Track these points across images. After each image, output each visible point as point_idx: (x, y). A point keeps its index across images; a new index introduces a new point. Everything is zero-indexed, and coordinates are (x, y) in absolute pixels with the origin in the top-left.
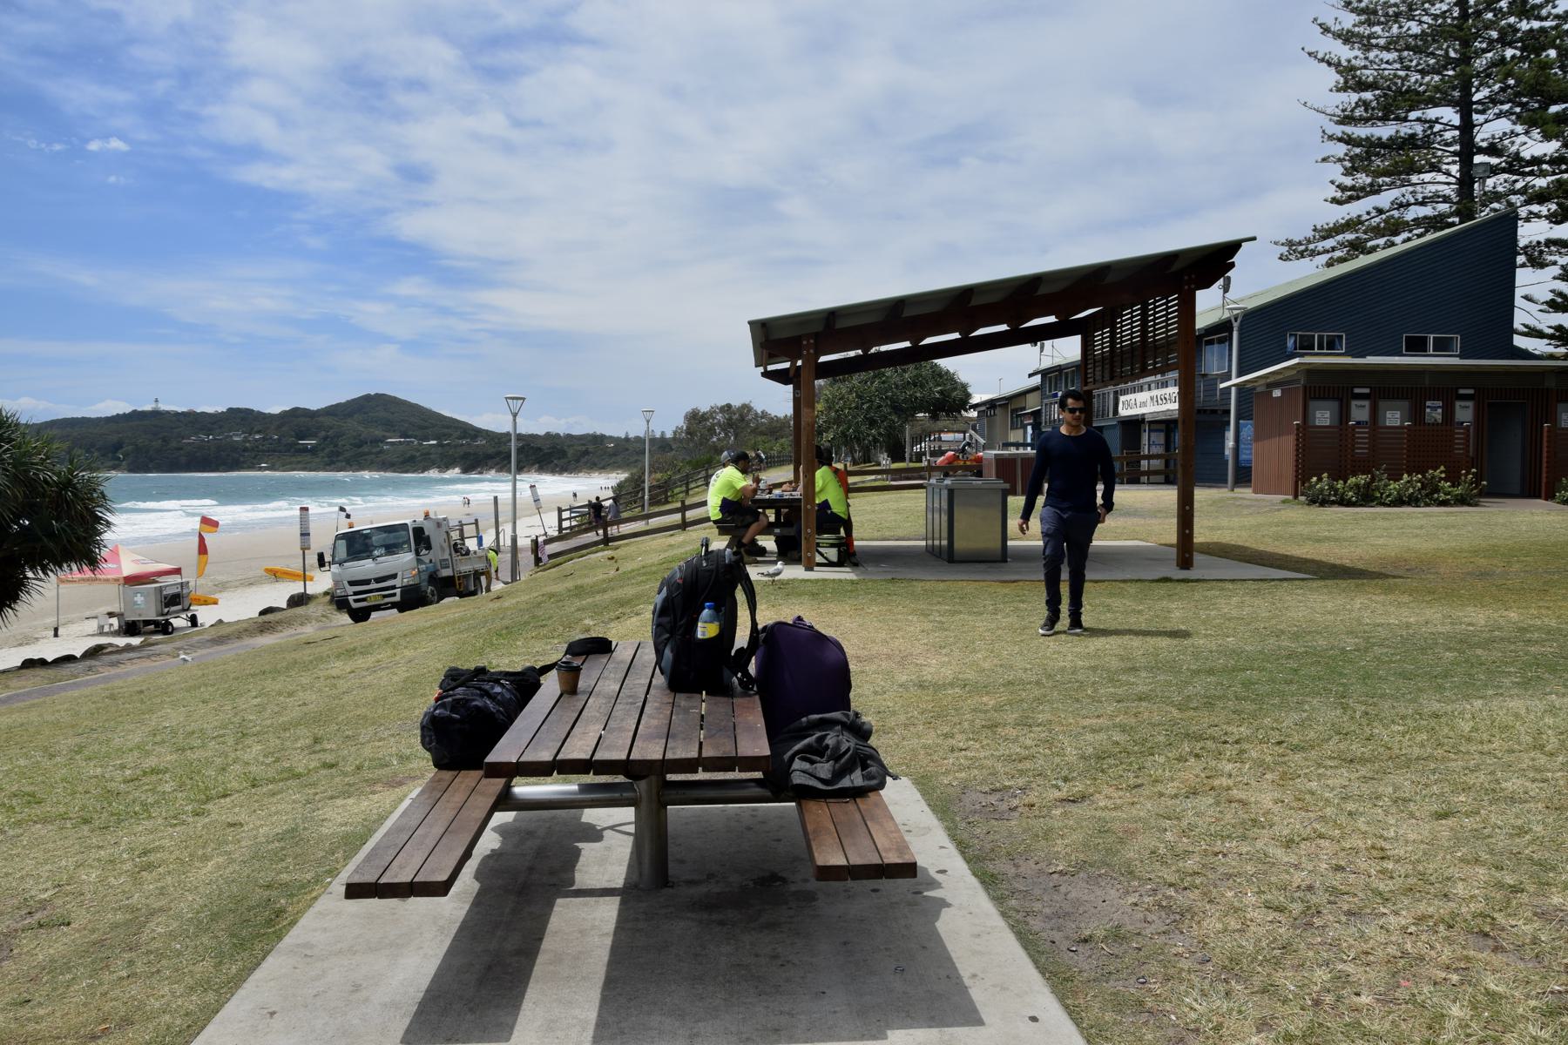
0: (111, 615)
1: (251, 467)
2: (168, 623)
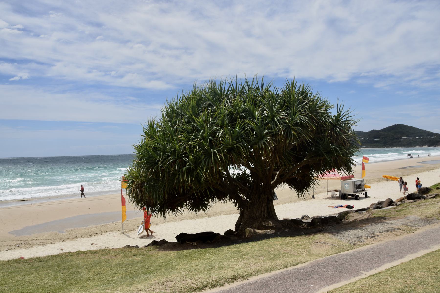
0: (336, 191)
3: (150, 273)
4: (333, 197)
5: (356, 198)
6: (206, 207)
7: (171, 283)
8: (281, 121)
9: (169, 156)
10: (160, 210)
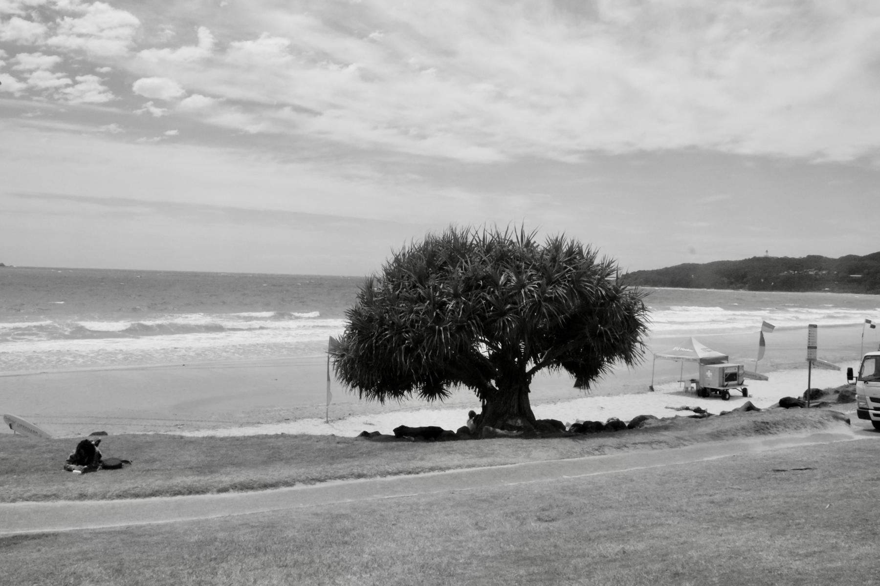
0: (693, 381)
1: (819, 290)
2: (726, 392)
3: (351, 457)
4: (686, 392)
5: (724, 395)
6: (444, 394)
7: (369, 467)
8: (529, 295)
9: (386, 330)
10: (377, 393)
